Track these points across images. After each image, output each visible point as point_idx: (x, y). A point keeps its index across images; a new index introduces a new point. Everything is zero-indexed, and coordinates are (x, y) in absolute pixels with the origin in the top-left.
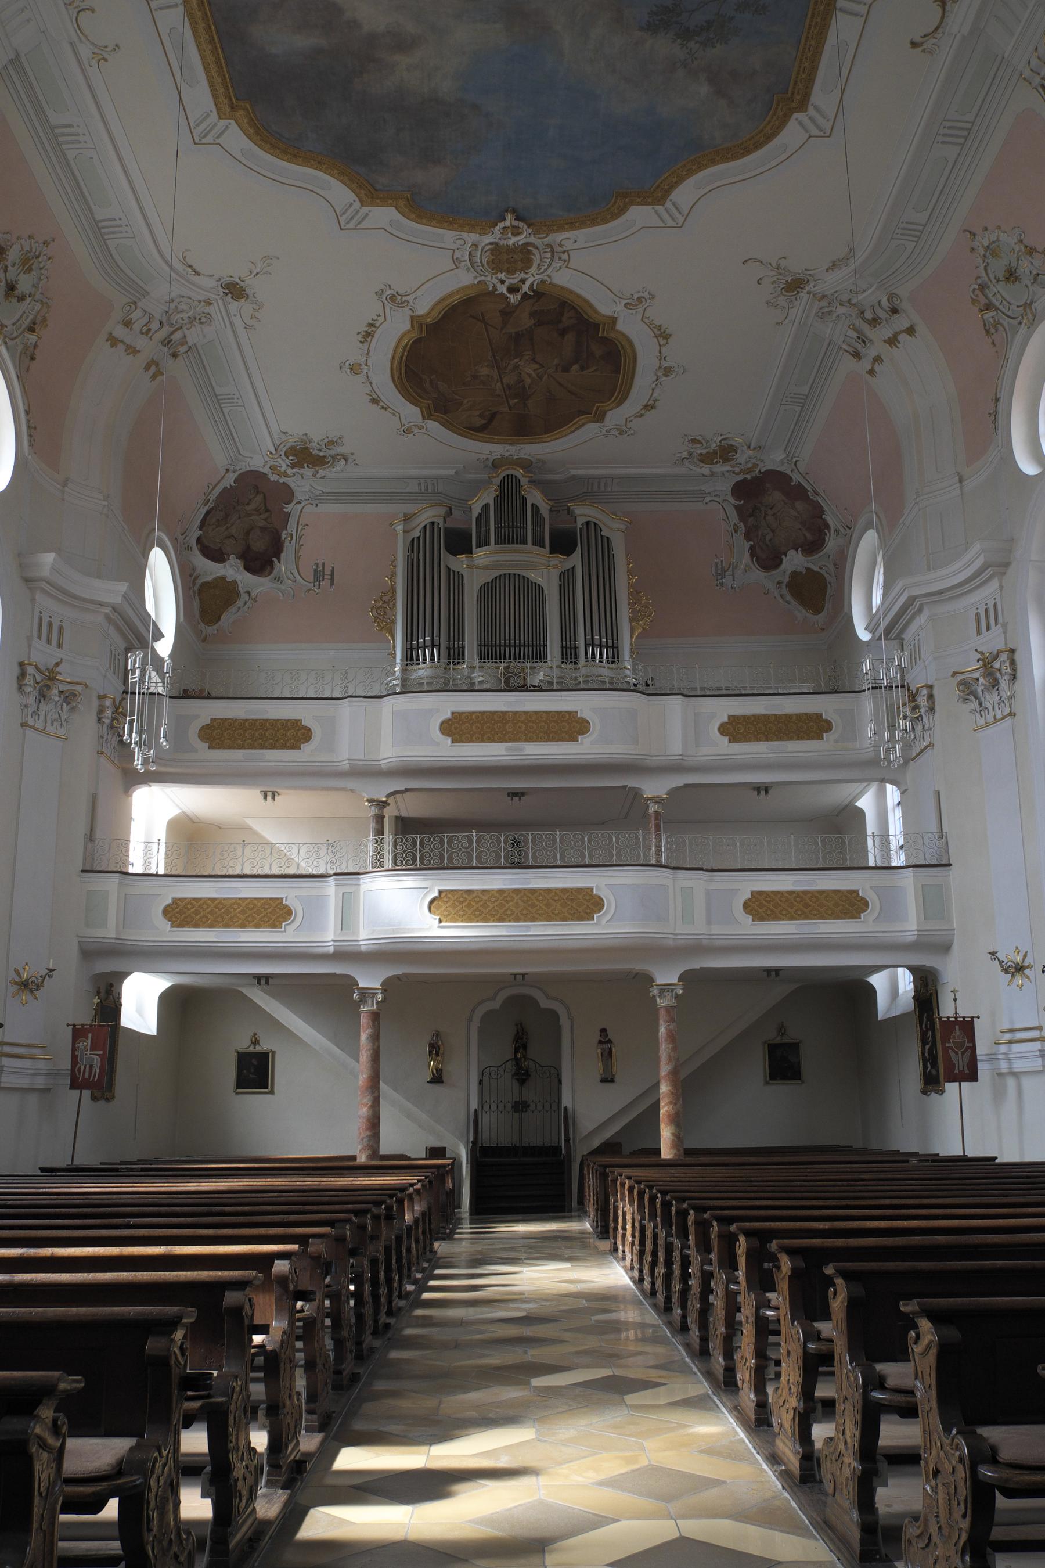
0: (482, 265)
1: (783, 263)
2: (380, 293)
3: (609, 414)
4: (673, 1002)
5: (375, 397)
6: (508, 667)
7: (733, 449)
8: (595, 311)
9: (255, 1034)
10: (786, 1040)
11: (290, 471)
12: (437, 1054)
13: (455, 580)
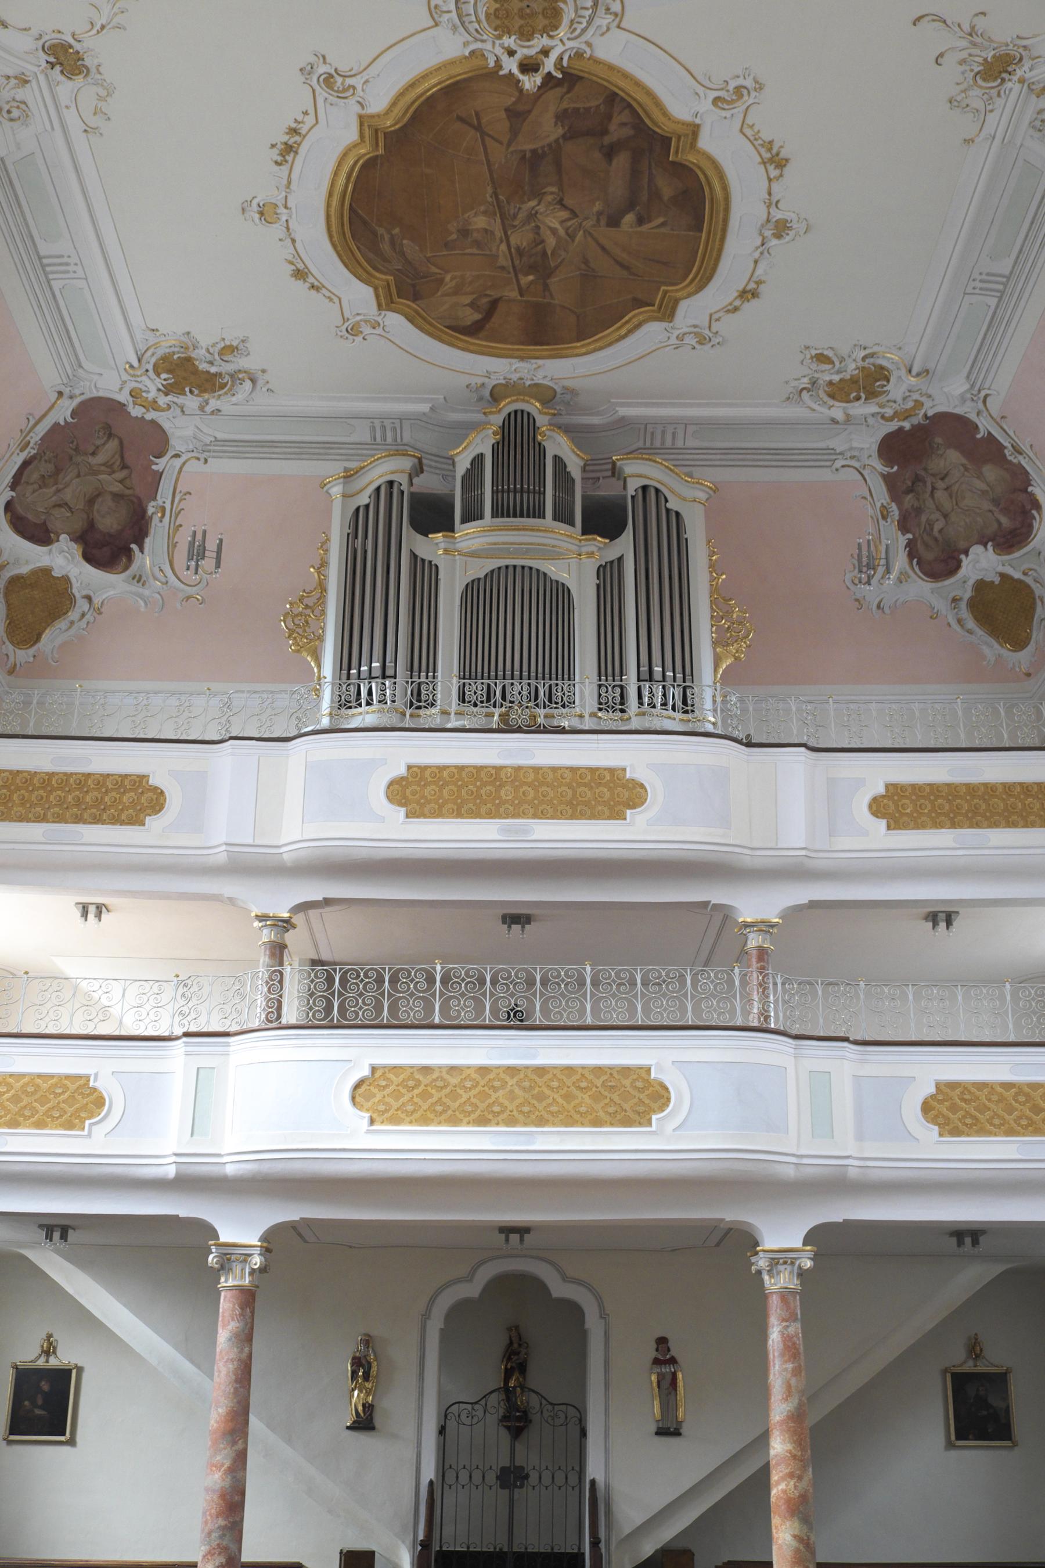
0: (479, 22)
1: (981, 23)
2: (306, 71)
3: (683, 306)
4: (794, 1284)
5: (301, 266)
6: (507, 714)
7: (882, 374)
8: (665, 113)
9: (49, 1336)
10: (981, 1368)
11: (163, 400)
12: (366, 1377)
13: (426, 575)
